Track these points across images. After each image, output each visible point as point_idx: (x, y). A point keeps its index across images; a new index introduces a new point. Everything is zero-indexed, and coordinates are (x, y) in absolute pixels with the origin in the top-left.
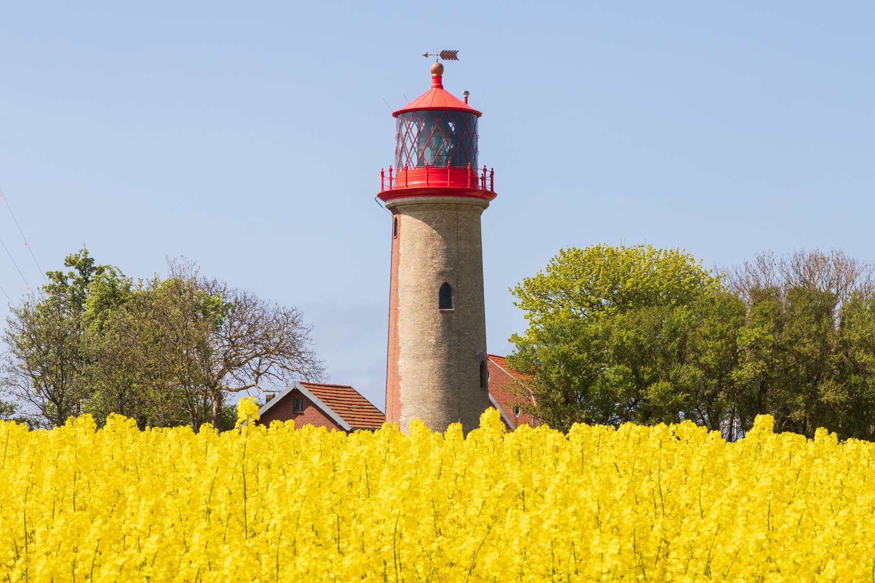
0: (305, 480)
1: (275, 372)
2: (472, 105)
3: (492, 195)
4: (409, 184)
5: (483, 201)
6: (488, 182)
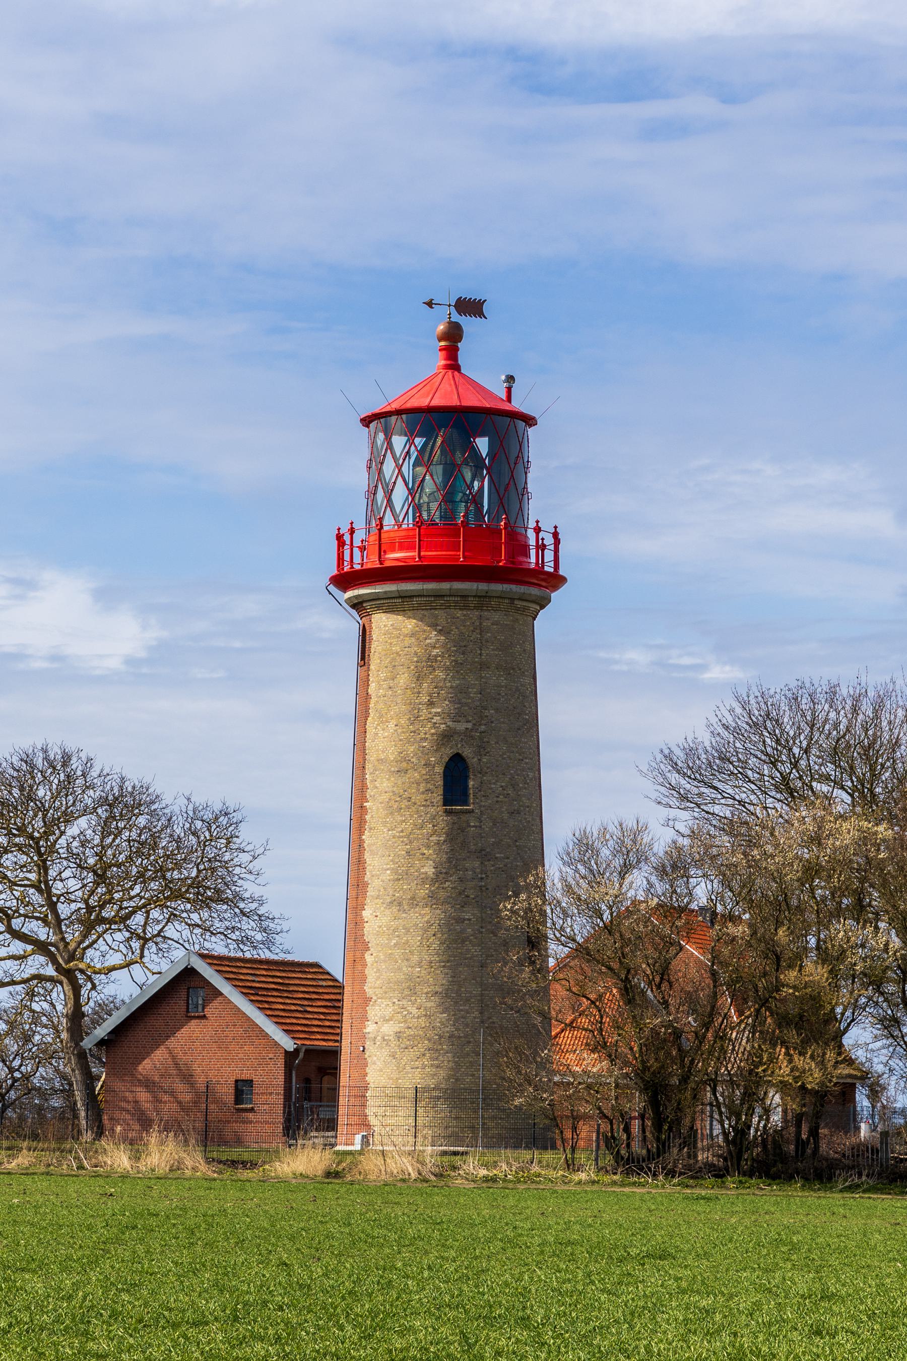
1: (176, 936)
2: (518, 404)
3: (556, 580)
5: (534, 591)
6: (549, 555)
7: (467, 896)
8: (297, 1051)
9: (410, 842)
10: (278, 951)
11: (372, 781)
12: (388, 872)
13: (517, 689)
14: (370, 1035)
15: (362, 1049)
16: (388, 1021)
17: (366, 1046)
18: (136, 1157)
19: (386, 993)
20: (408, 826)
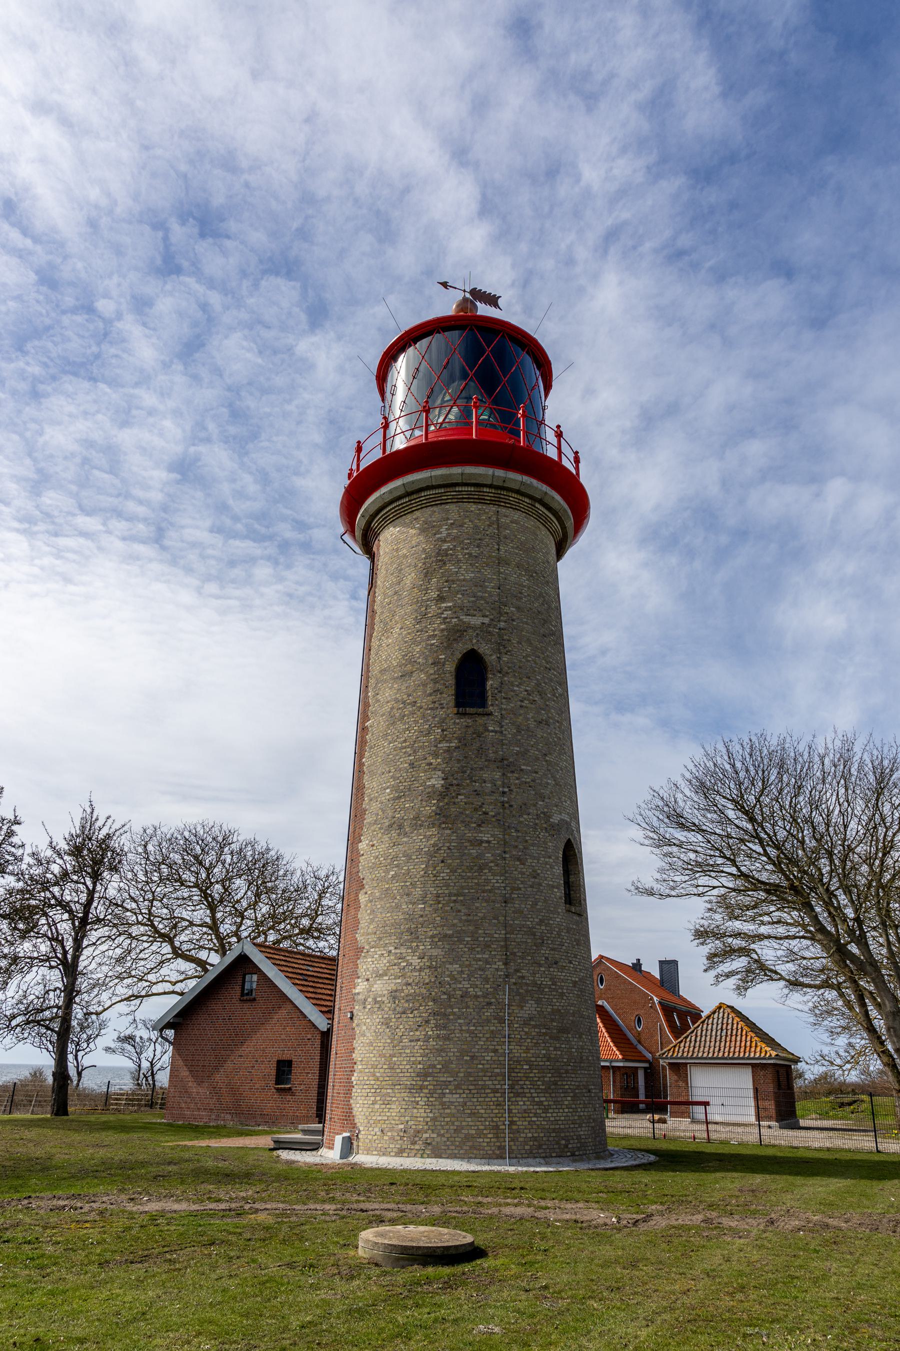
0: (195, 937)
7: (486, 813)
9: (415, 752)
12: (388, 791)
15: (349, 1015)
16: (381, 976)
19: (380, 939)
20: (412, 734)
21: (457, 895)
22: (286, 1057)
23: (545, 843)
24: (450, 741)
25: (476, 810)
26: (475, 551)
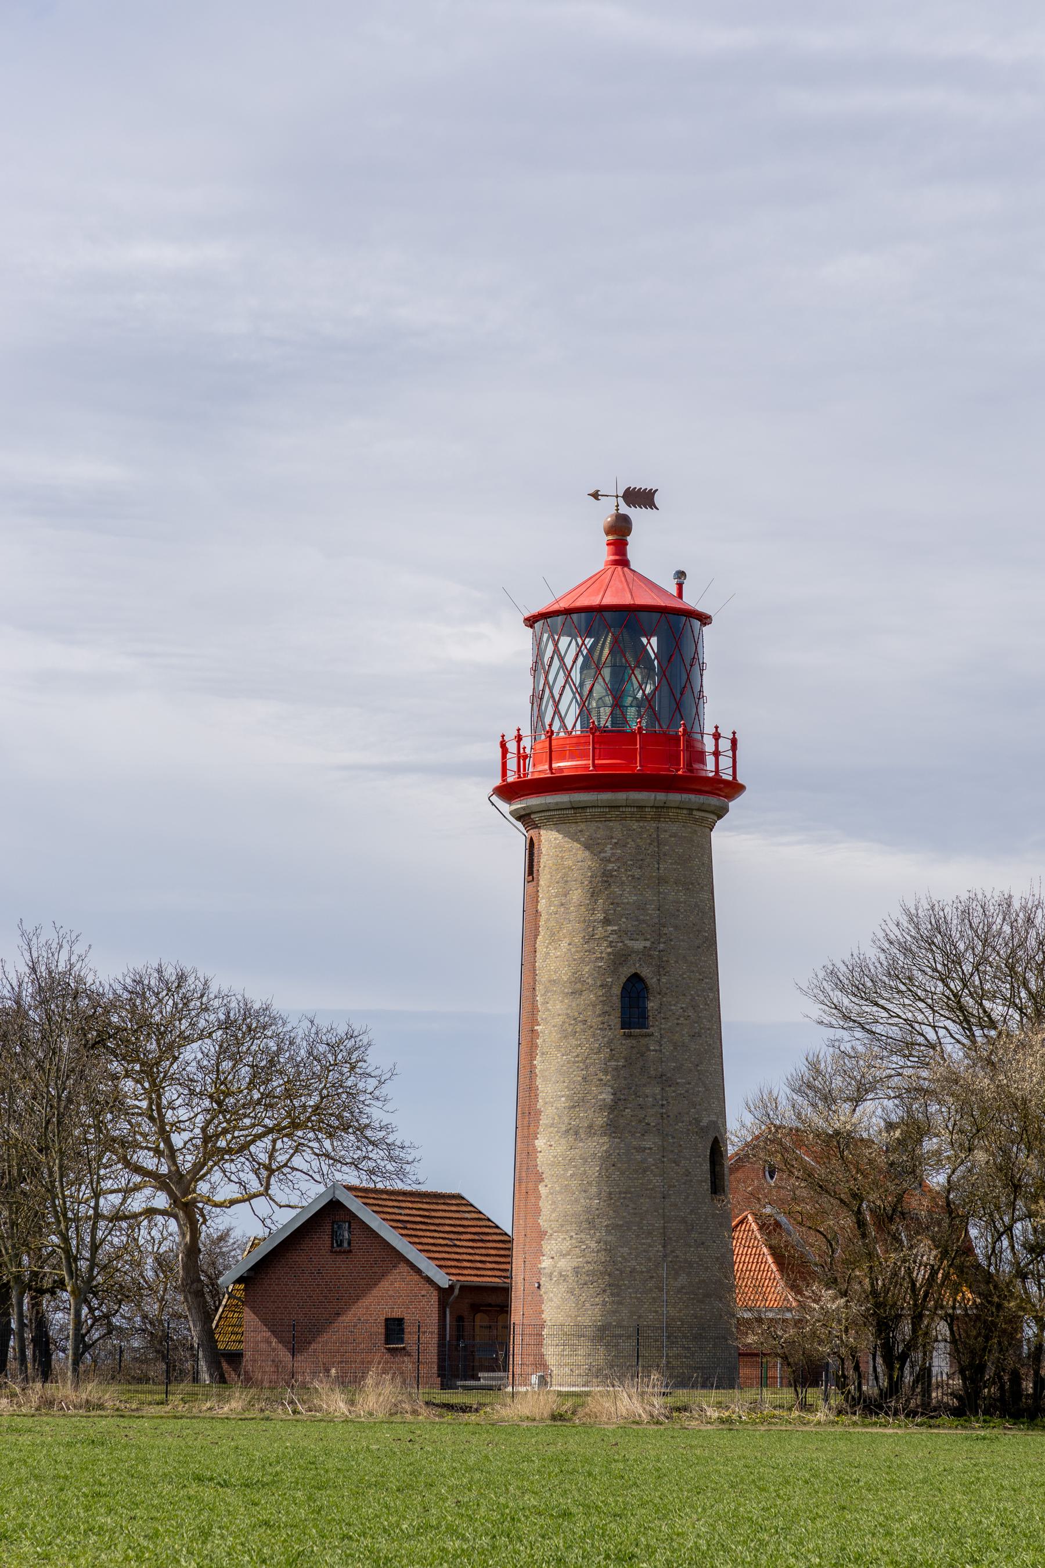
1: (305, 1167)
2: (691, 600)
3: (734, 788)
4: (555, 765)
5: (713, 801)
6: (725, 762)
7: (648, 1124)
8: (452, 1287)
10: (410, 1182)
11: (543, 1003)
13: (696, 905)
14: (546, 1271)
16: (564, 1255)
17: (542, 1283)
18: (352, 1403)
19: (562, 1226)
21: (625, 1193)
22: (396, 1314)
23: (696, 1145)
24: (617, 1061)
25: (640, 1121)
26: (637, 873)
